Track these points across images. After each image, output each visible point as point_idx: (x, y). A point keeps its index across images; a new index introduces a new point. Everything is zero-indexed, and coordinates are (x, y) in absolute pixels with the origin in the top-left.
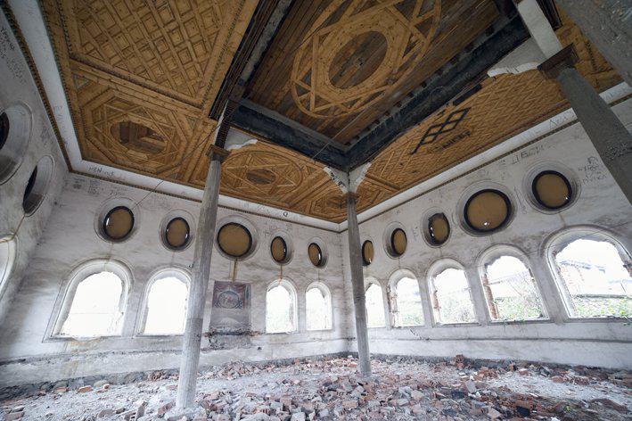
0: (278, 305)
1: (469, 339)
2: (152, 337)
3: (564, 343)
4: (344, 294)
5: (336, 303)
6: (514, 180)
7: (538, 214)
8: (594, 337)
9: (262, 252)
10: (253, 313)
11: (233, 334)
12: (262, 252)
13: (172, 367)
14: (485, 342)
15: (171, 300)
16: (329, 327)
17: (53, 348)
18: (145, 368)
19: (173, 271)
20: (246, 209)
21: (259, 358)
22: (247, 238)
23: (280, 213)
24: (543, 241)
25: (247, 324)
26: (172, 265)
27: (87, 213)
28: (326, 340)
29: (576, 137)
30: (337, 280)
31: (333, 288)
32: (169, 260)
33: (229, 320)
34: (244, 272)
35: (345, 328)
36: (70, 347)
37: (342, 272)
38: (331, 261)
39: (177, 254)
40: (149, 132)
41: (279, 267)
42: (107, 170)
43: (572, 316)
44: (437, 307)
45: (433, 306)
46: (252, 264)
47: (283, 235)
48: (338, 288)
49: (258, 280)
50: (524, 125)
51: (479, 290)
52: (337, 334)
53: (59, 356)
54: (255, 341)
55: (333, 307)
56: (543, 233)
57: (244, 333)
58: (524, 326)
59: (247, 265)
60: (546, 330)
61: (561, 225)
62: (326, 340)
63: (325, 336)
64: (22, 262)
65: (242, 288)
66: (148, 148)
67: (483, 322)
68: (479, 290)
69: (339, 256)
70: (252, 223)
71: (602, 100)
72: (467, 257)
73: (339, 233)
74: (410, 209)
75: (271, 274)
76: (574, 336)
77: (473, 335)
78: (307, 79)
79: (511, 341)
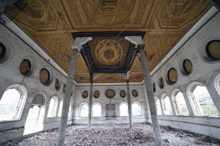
0: (123, 109)
1: (172, 121)
2: (94, 117)
3: (193, 125)
4: (146, 104)
5: (143, 107)
6: (177, 64)
7: (183, 77)
8: (201, 123)
9: (118, 95)
10: (116, 111)
11: (112, 116)
12: (118, 95)
13: (98, 123)
14: (174, 122)
15: (97, 110)
16: (141, 115)
17: (79, 118)
18: (93, 123)
19: (97, 103)
20: (112, 85)
21: (118, 123)
22: (114, 92)
23: (121, 84)
24: (186, 86)
25: (115, 114)
26: (96, 102)
27: (80, 95)
28: (139, 119)
29: (189, 47)
30: (142, 100)
31: (141, 103)
32: (95, 101)
33: (111, 113)
34: (113, 101)
35: (146, 115)
36: (81, 118)
37: (145, 97)
38: (140, 94)
39: (97, 99)
40: (84, 77)
41: (122, 98)
42: (81, 84)
43: (197, 115)
44: (165, 109)
45: (163, 109)
46: (115, 99)
47: (123, 89)
48: (143, 102)
49: (117, 103)
50: (172, 46)
51: (173, 103)
52: (143, 116)
53: (80, 120)
54: (117, 118)
55: (141, 109)
56: (185, 84)
57: (114, 116)
58: (184, 118)
59: (114, 99)
60: (190, 120)
61: (189, 81)
62: (139, 119)
63: (139, 117)
64: (73, 104)
65: (114, 105)
66: (85, 79)
67: (174, 115)
68: (173, 103)
69: (143, 92)
70: (114, 88)
71: (51, 117)
72: (168, 93)
73: (142, 85)
74: (157, 74)
75: (120, 101)
76: (196, 123)
77: (172, 119)
78: (102, 60)
79: (180, 123)
